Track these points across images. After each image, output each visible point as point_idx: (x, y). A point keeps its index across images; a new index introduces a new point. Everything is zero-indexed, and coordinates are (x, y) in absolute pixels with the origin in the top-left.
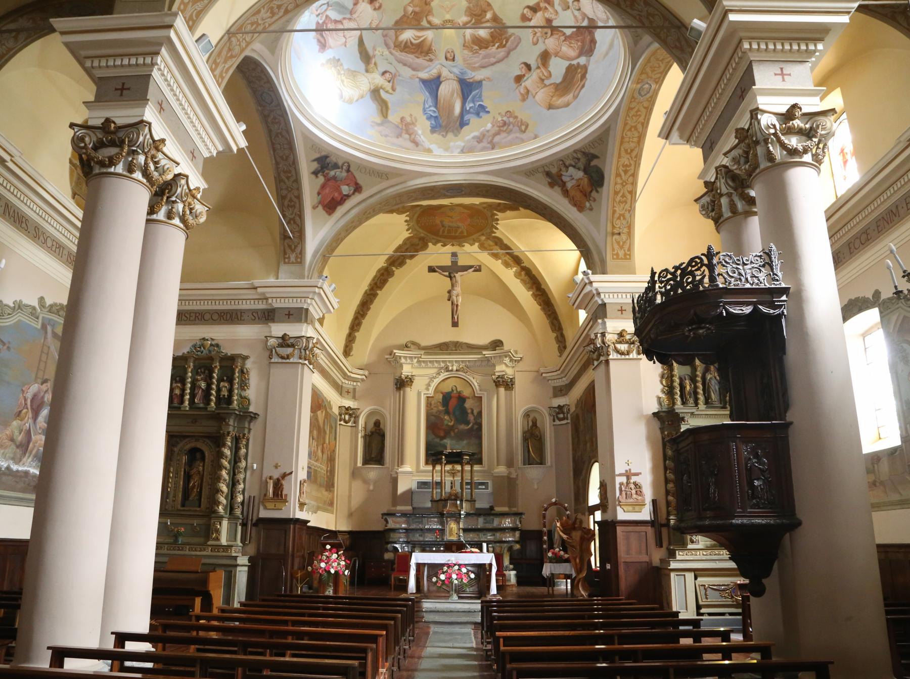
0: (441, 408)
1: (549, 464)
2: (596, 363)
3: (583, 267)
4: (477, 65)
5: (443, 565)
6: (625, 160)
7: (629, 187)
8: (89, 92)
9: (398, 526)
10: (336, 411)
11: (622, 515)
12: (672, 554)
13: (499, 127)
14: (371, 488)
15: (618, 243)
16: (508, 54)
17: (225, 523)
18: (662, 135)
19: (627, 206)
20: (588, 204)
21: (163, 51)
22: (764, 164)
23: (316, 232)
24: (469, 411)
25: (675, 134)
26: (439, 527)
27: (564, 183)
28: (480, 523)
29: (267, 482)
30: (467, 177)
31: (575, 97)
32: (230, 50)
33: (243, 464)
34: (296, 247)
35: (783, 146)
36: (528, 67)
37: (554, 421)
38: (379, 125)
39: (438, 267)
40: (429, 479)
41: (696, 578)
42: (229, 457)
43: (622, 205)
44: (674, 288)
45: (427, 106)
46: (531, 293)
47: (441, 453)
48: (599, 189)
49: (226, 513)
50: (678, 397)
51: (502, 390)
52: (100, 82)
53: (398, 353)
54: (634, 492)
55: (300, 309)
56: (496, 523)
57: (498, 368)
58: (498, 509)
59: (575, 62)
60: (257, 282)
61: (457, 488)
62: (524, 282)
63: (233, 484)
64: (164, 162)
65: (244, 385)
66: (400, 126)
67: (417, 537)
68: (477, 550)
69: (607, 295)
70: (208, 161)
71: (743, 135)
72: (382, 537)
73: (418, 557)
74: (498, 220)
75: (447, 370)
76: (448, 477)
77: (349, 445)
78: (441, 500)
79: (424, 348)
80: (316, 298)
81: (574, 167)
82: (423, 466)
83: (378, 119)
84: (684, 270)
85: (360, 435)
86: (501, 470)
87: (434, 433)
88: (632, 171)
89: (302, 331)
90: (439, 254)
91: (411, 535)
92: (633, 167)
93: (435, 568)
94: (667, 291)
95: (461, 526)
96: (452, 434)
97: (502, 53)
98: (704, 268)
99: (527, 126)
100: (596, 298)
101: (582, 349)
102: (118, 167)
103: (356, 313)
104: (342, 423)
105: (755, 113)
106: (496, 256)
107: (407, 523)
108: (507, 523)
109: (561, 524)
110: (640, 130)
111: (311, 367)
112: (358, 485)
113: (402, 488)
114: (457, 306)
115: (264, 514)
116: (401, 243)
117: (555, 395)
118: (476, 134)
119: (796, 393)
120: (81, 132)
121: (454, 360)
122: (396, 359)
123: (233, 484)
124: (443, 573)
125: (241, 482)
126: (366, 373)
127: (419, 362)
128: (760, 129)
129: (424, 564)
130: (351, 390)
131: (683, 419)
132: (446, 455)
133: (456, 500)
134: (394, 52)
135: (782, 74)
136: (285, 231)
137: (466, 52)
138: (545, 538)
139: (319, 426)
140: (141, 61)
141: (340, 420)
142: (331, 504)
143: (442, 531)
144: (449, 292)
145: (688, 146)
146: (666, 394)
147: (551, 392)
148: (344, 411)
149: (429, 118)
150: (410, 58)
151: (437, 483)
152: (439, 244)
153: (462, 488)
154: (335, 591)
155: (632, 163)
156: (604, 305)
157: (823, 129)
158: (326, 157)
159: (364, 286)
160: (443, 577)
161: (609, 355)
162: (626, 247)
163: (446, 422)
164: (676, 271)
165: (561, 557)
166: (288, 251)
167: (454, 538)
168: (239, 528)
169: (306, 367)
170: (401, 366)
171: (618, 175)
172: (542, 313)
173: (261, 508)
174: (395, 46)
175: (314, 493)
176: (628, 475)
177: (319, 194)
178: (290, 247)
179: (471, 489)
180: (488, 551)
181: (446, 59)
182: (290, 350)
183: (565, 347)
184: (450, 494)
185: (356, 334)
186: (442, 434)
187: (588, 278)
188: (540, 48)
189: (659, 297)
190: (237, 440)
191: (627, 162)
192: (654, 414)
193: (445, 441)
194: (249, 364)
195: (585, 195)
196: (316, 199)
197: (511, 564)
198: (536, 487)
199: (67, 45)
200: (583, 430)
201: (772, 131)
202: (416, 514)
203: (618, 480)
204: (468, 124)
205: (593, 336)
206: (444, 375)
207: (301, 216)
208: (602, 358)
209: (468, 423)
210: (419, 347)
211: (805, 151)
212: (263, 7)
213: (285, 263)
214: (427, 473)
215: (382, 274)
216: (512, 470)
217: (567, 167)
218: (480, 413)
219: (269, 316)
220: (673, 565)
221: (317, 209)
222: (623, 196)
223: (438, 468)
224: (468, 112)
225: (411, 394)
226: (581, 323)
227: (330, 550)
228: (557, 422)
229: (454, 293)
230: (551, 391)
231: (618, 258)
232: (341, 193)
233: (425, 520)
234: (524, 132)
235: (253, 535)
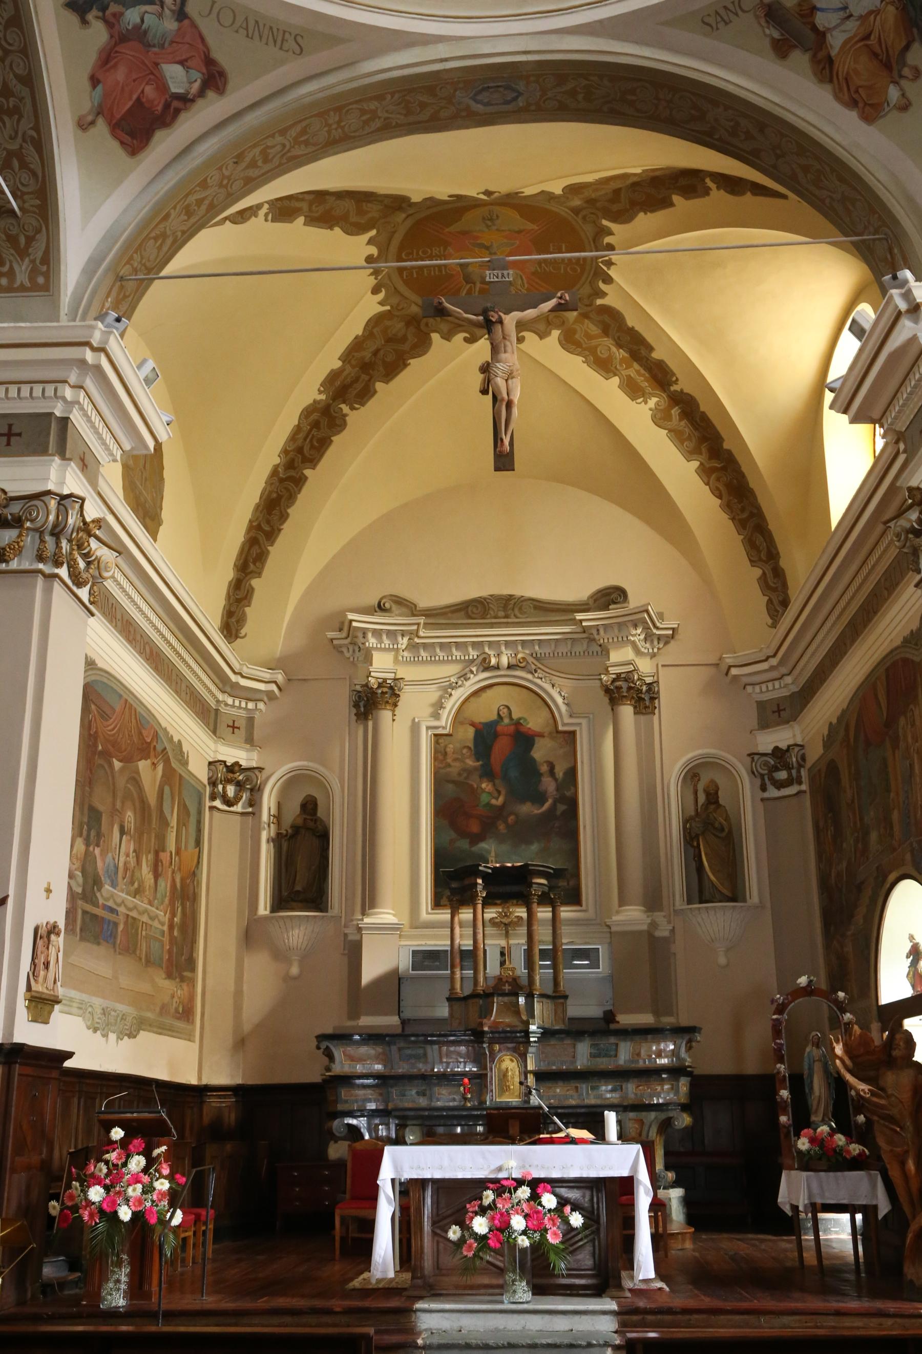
0: (471, 763)
5: (481, 1184)
9: (359, 1068)
10: (199, 770)
14: (295, 970)
18: (838, 404)
20: (893, 93)
24: (544, 768)
26: (471, 1068)
28: (582, 1055)
30: (533, 45)
34: (30, 240)
37: (763, 788)
40: (442, 944)
46: (695, 464)
47: (473, 871)
51: (627, 711)
53: (359, 621)
56: (625, 1054)
57: (616, 656)
58: (625, 1019)
62: (677, 436)
67: (412, 1098)
68: (585, 1134)
72: (317, 1100)
73: (401, 1163)
76: (496, 939)
77: (233, 863)
78: (474, 996)
79: (429, 613)
80: (89, 383)
82: (426, 913)
86: (632, 916)
87: (453, 825)
91: (394, 1092)
93: (458, 1196)
95: (530, 1067)
96: (502, 827)
101: (880, 528)
103: (250, 528)
104: (218, 803)
106: (604, 366)
107: (386, 1060)
108: (663, 1052)
109: (847, 1049)
112: (259, 965)
113: (370, 971)
114: (509, 405)
116: (359, 330)
117: (764, 725)
121: (504, 640)
124: (483, 1211)
126: (280, 677)
129: (422, 1183)
130: (241, 723)
132: (485, 876)
133: (517, 995)
138: (785, 1093)
139: (143, 801)
141: (213, 798)
142: (186, 1013)
143: (480, 1080)
144: (485, 369)
147: (752, 719)
148: (221, 771)
151: (464, 954)
152: (460, 336)
154: (137, 1288)
159: (270, 455)
160: (480, 1225)
163: (484, 798)
165: (838, 1152)
167: (512, 1099)
169: (57, 586)
170: (368, 659)
172: (724, 517)
175: (125, 981)
177: (94, 81)
178: (12, 240)
179: (555, 966)
180: (623, 1137)
183: (785, 603)
184: (499, 979)
185: (255, 582)
186: (475, 828)
193: (483, 845)
195: (887, 66)
196: (88, 101)
198: (722, 960)
202: (413, 1035)
207: (40, 143)
209: (540, 798)
210: (411, 609)
212: (174, 208)
214: (440, 928)
215: (316, 425)
216: (659, 917)
218: (572, 773)
221: (93, 131)
223: (466, 915)
226: (834, 522)
227: (124, 1143)
228: (773, 792)
229: (500, 368)
230: (753, 713)
232: (162, 86)
233: (432, 1051)
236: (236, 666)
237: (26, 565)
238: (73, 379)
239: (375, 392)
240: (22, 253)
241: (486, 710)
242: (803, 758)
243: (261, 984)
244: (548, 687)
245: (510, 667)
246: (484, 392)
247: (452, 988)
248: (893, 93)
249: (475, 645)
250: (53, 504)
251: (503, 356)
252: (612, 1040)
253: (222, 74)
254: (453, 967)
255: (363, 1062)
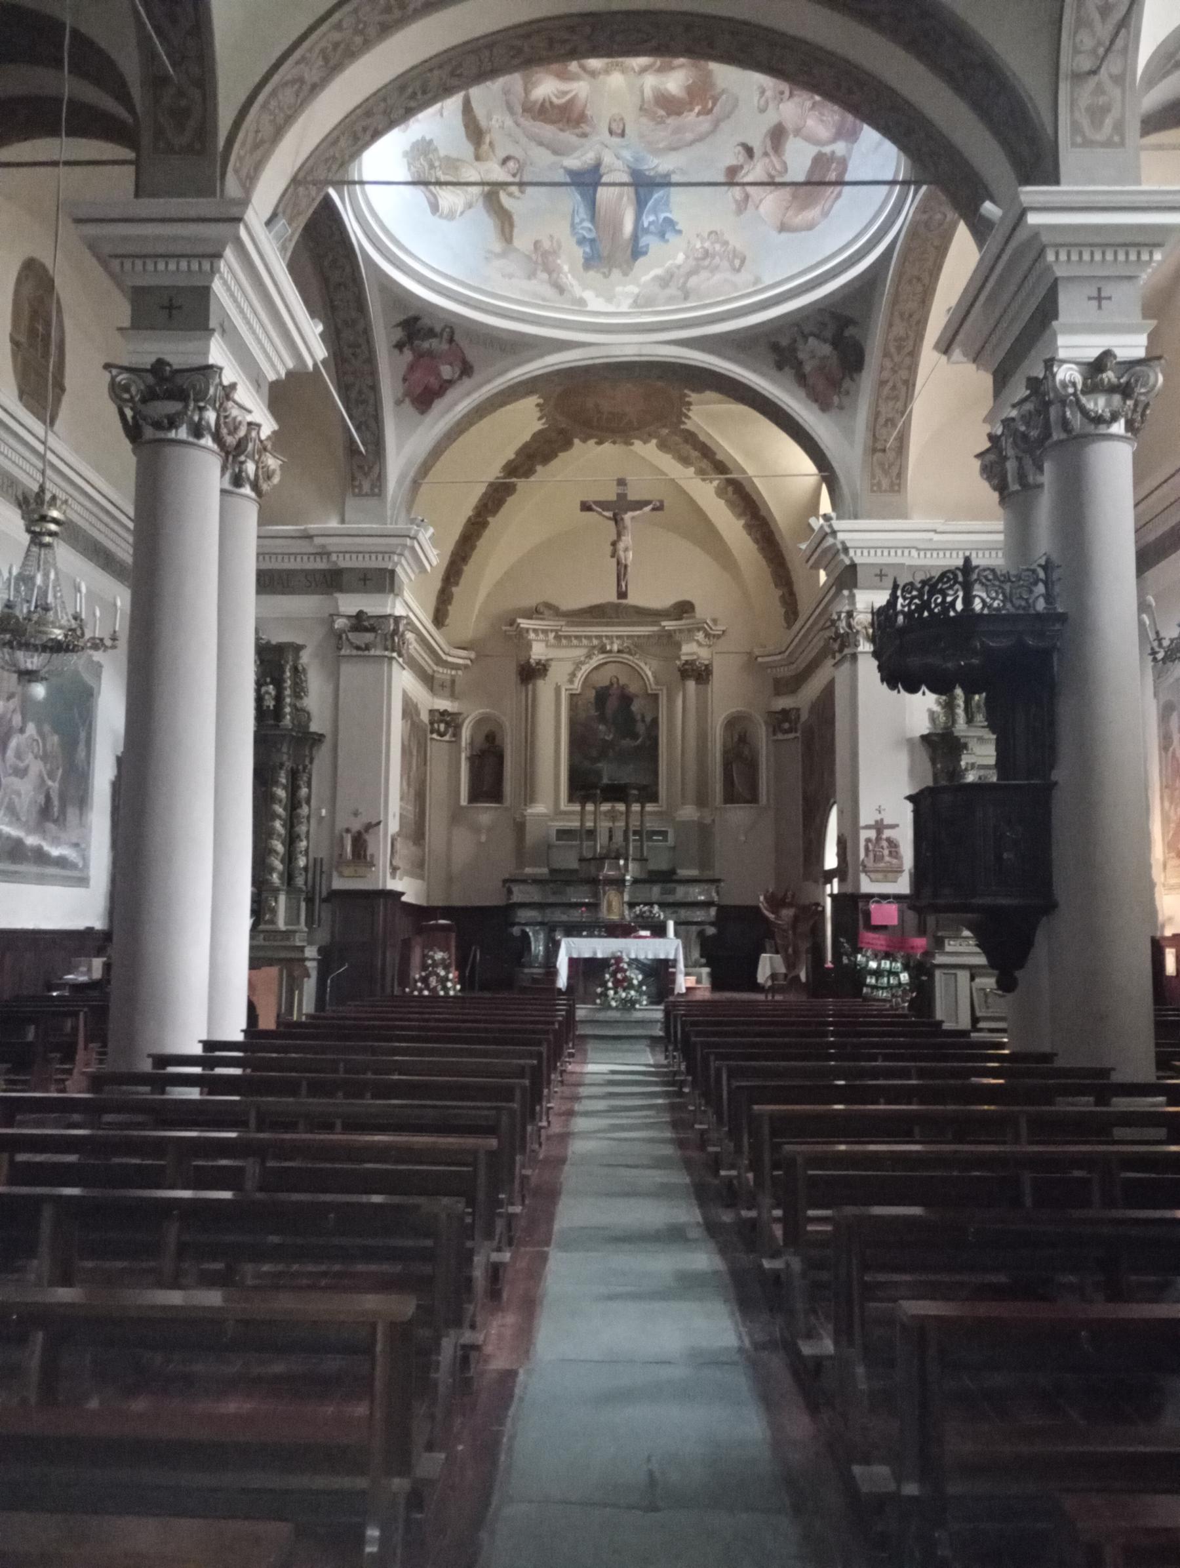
1: (763, 799)
2: (838, 656)
3: (825, 506)
4: (661, 146)
6: (899, 329)
7: (904, 374)
8: (123, 312)
10: (425, 717)
11: (867, 886)
12: (939, 943)
13: (697, 259)
14: (483, 838)
15: (881, 465)
16: (716, 125)
17: (282, 898)
19: (899, 405)
20: (836, 399)
21: (229, 253)
22: (1057, 435)
23: (404, 444)
24: (639, 717)
25: (957, 354)
27: (800, 363)
29: (342, 839)
31: (825, 214)
32: (295, 205)
33: (304, 810)
34: (370, 468)
35: (1084, 412)
36: (749, 151)
38: (499, 256)
39: (596, 503)
40: (576, 824)
41: (972, 978)
42: (284, 801)
43: (891, 404)
44: (920, 609)
45: (577, 220)
46: (742, 522)
48: (855, 376)
49: (283, 883)
50: (960, 712)
51: (691, 685)
52: (139, 296)
53: (524, 623)
54: (886, 852)
55: (383, 571)
58: (683, 873)
59: (827, 150)
60: (313, 527)
61: (619, 837)
62: (731, 504)
63: (291, 840)
64: (235, 412)
65: (299, 690)
66: (534, 257)
67: (560, 916)
69: (859, 552)
70: (275, 386)
71: (1034, 384)
74: (690, 404)
75: (603, 650)
76: (604, 818)
78: (594, 859)
80: (407, 553)
81: (815, 335)
82: (564, 805)
83: (497, 247)
84: (935, 584)
85: (463, 756)
86: (688, 812)
88: (910, 348)
89: (386, 606)
90: (591, 465)
92: (911, 343)
94: (911, 612)
97: (705, 124)
98: (957, 586)
99: (743, 261)
100: (842, 556)
102: (180, 430)
104: (435, 736)
105: (1050, 363)
106: (685, 461)
109: (765, 898)
110: (926, 281)
111: (401, 660)
114: (626, 566)
115: (338, 884)
118: (658, 271)
119: (1066, 748)
120: (122, 378)
121: (616, 633)
122: (521, 633)
123: (291, 840)
125: (303, 836)
127: (558, 637)
128: (1054, 386)
131: (965, 746)
134: (522, 120)
135: (1099, 298)
136: (352, 440)
137: (644, 120)
140: (195, 266)
141: (432, 732)
144: (614, 544)
145: (974, 367)
146: (943, 707)
149: (581, 241)
150: (548, 131)
152: (592, 442)
153: (626, 839)
155: (912, 334)
156: (853, 567)
157: (1143, 386)
158: (416, 319)
159: (467, 510)
161: (857, 646)
162: (895, 471)
164: (923, 587)
166: (359, 476)
167: (615, 917)
168: (303, 905)
169: (394, 663)
170: (529, 646)
171: (886, 354)
172: (760, 557)
173: (335, 874)
174: (524, 110)
176: (879, 827)
177: (405, 380)
179: (641, 840)
181: (611, 132)
182: (369, 637)
185: (454, 589)
187: (830, 526)
188: (771, 118)
189: (901, 618)
190: (294, 775)
191: (902, 333)
192: (924, 738)
193: (600, 765)
194: (305, 658)
197: (702, 956)
199: (93, 246)
200: (815, 754)
201: (1071, 390)
203: (864, 835)
204: (645, 253)
205: (835, 617)
206: (597, 659)
207: (378, 419)
208: (847, 651)
209: (635, 736)
211: (1114, 418)
213: (355, 495)
214: (571, 815)
217: (805, 337)
219: (332, 581)
220: (939, 959)
222: (894, 388)
223: (590, 807)
224: (646, 231)
225: (544, 689)
228: (780, 736)
229: (621, 546)
231: (880, 490)
233: (570, 890)
234: (739, 270)
235: (323, 915)
236: (447, 650)
237: (378, 653)
238: (398, 551)
239: (536, 471)
240: (366, 475)
241: (603, 679)
242: (799, 717)
243: (464, 846)
244: (642, 665)
245: (619, 651)
246: (613, 556)
247: (581, 853)
248: (836, 399)
249: (597, 637)
250: (392, 621)
251: (623, 538)
252: (673, 885)
253: (471, 368)
254: (581, 840)
255: (530, 894)
